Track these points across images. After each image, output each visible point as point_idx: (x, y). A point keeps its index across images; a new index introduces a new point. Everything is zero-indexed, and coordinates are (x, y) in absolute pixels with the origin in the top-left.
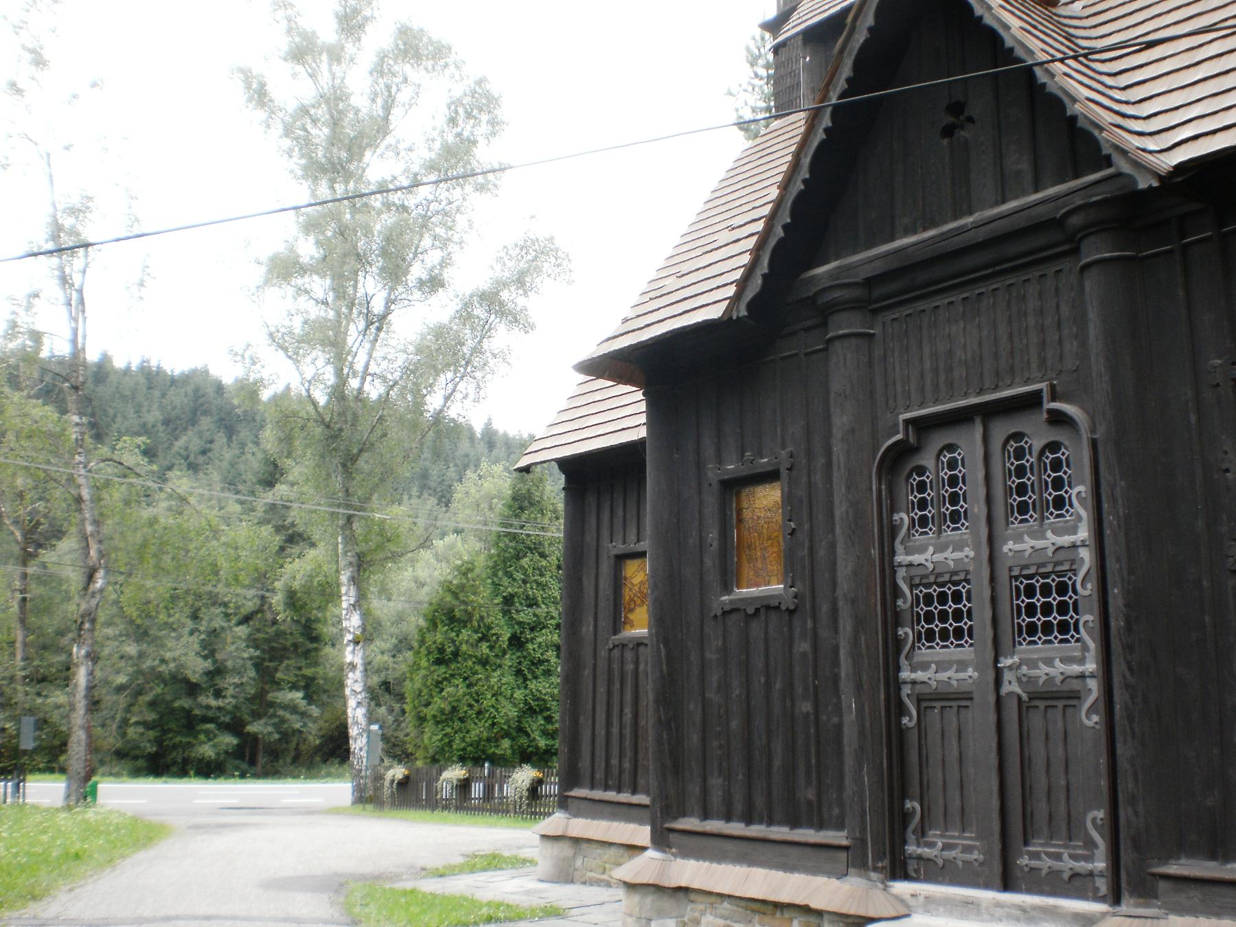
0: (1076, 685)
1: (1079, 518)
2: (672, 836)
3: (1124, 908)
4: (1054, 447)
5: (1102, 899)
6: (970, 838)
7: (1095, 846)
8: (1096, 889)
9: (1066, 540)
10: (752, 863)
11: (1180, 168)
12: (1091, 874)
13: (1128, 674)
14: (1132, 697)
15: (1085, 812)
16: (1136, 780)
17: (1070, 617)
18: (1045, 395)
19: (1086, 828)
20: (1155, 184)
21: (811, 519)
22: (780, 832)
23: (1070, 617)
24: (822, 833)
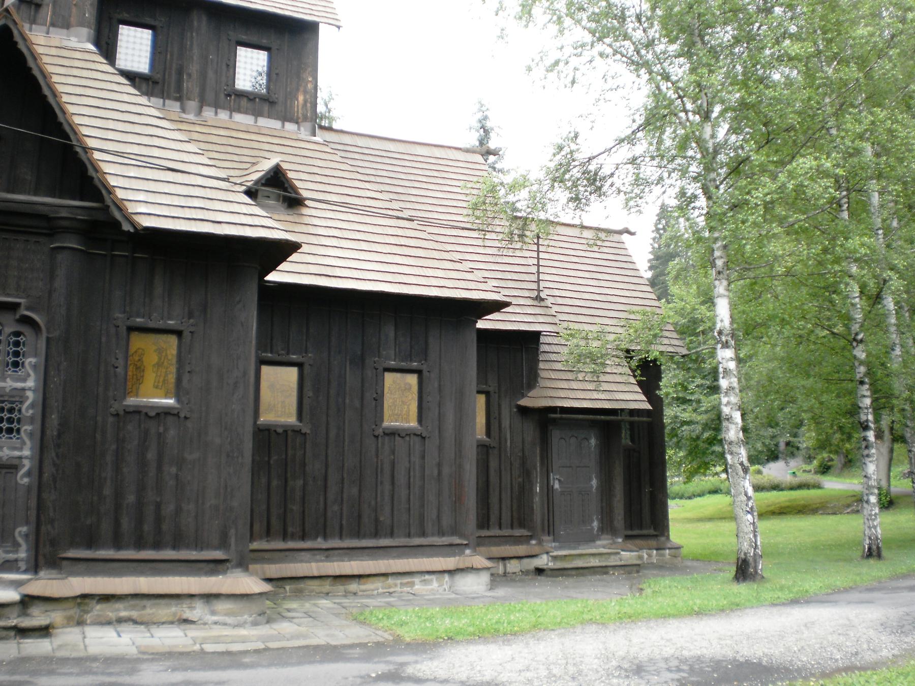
0: (15, 462)
1: (29, 375)
2: (65, 563)
3: (42, 574)
4: (17, 334)
5: (26, 571)
6: (604, 547)
7: (19, 545)
8: (19, 568)
9: (19, 385)
10: (432, 556)
11: (147, 229)
12: (16, 560)
13: (55, 459)
14: (57, 470)
15: (14, 529)
16: (55, 510)
17: (15, 425)
18: (22, 307)
19: (14, 537)
20: (132, 230)
21: (393, 483)
22: (193, 555)
23: (15, 425)
24: (203, 553)
